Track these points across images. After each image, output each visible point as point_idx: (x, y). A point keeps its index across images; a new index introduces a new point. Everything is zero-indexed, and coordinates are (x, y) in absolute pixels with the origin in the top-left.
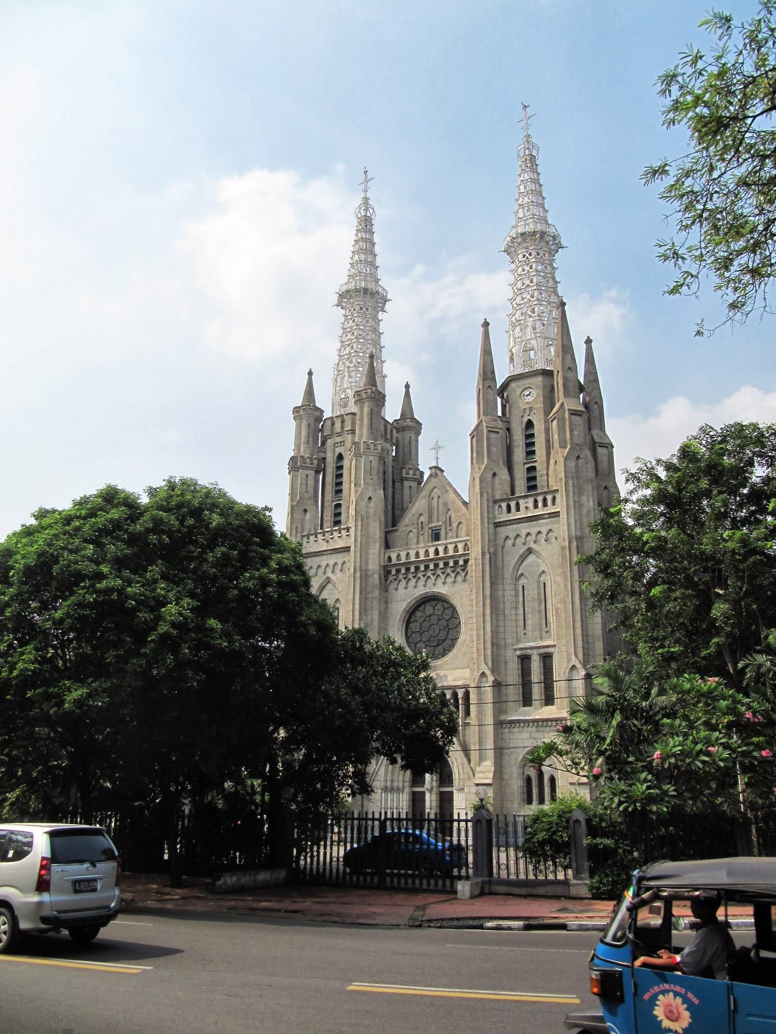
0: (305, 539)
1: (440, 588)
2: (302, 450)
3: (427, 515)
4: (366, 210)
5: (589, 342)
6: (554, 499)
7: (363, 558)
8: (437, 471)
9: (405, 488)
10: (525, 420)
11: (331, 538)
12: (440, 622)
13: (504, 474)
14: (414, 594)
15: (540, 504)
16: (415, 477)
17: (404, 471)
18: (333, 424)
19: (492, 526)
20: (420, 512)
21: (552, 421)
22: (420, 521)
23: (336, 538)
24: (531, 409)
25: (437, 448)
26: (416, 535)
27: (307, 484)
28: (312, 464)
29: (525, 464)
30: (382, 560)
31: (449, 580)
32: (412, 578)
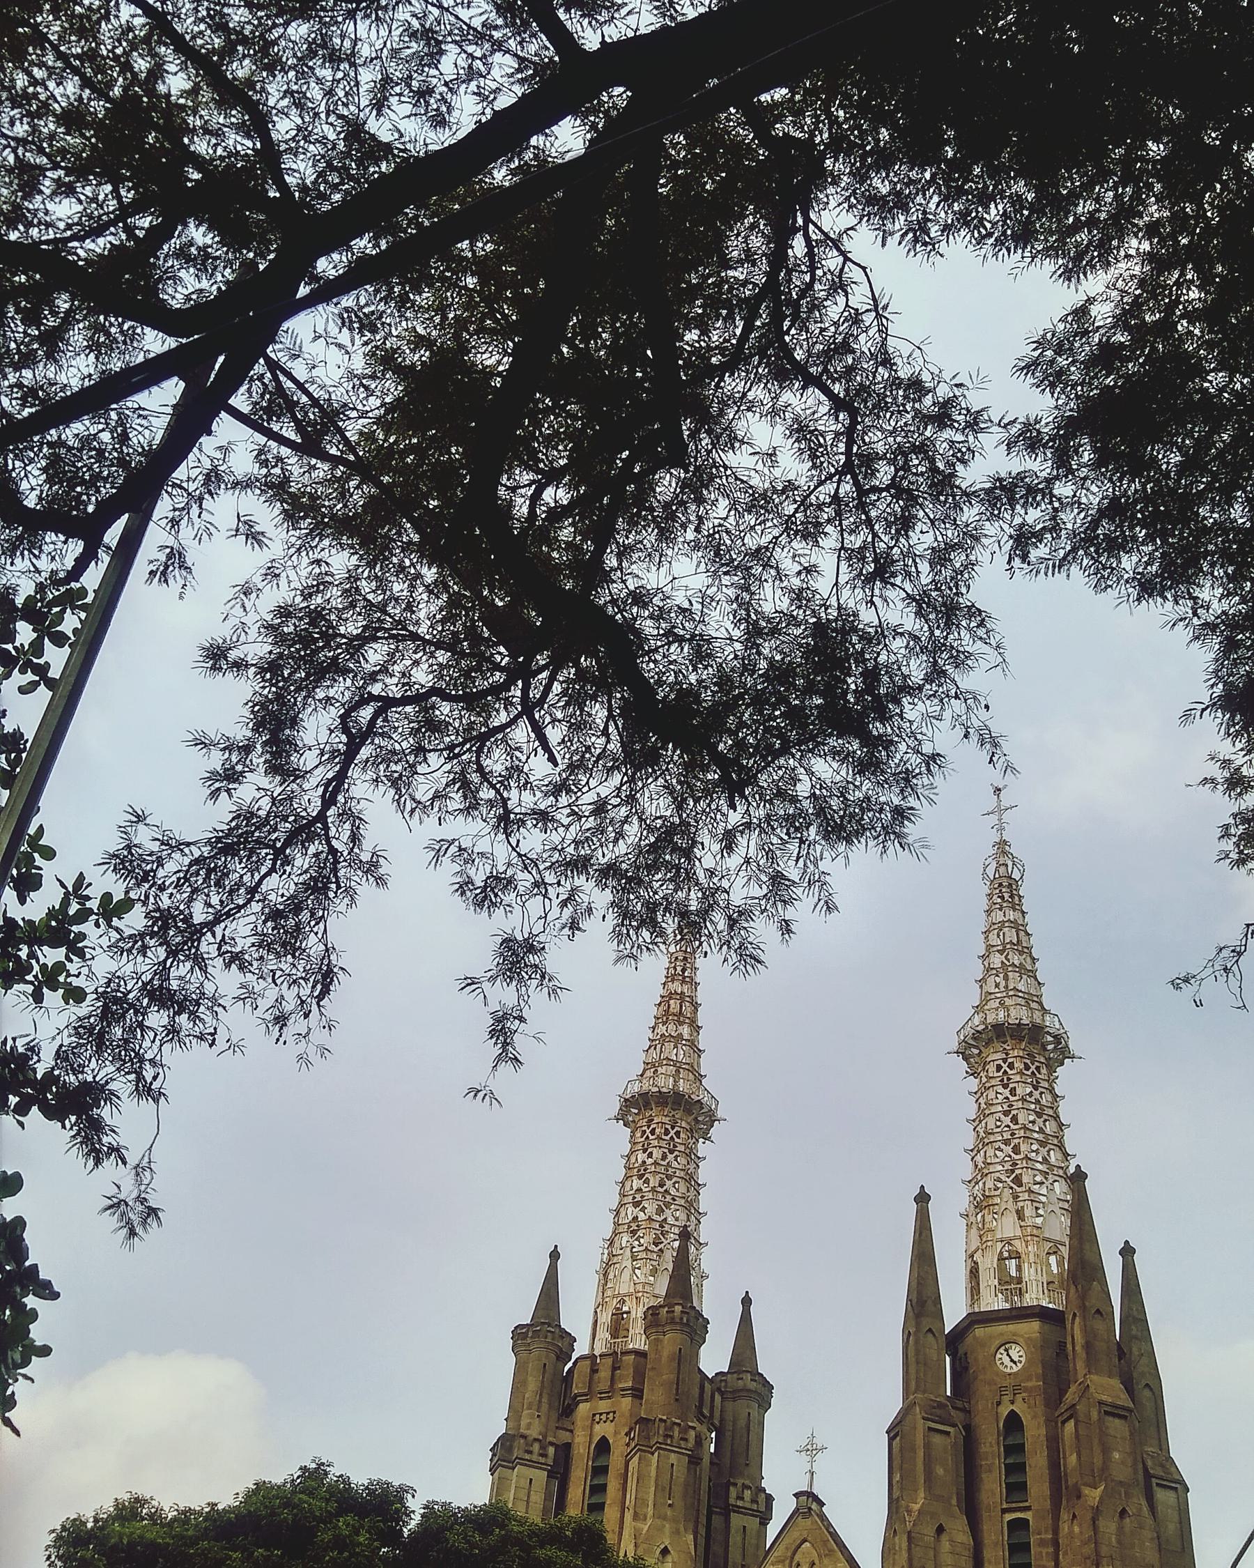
2: (524, 1423)
5: (1127, 1252)
8: (809, 1503)
9: (733, 1531)
10: (1004, 1411)
13: (959, 1531)
16: (542, 1460)
17: (733, 1492)
18: (594, 1371)
21: (1064, 1422)
25: (812, 1449)
27: (528, 1502)
28: (542, 1455)
29: (1004, 1511)
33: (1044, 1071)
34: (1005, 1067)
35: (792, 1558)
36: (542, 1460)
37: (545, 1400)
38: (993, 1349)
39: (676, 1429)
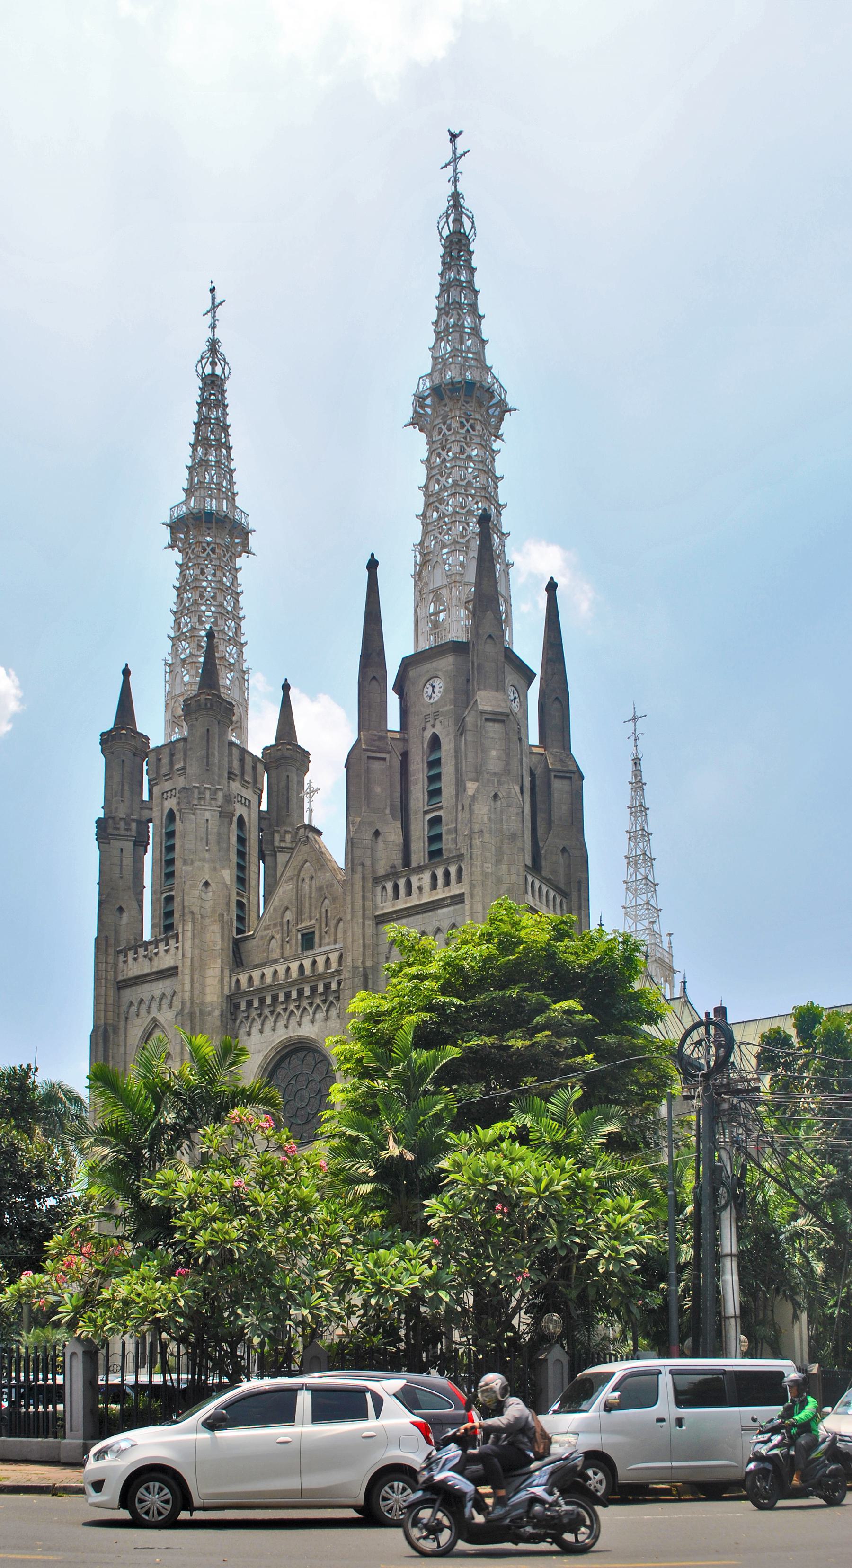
0: (121, 958)
1: (308, 1030)
3: (294, 909)
4: (214, 364)
6: (460, 871)
7: (196, 985)
10: (428, 735)
11: (156, 954)
12: (310, 1086)
14: (273, 1041)
15: (440, 881)
16: (128, 833)
17: (277, 837)
19: (369, 922)
20: (285, 905)
22: (285, 920)
23: (162, 953)
24: (436, 715)
26: (279, 942)
27: (121, 865)
28: (127, 830)
29: (426, 813)
30: (226, 988)
31: (320, 1016)
32: (269, 1014)
33: (478, 427)
34: (444, 429)
35: (298, 875)
36: (128, 833)
37: (126, 788)
38: (422, 684)
39: (208, 793)
